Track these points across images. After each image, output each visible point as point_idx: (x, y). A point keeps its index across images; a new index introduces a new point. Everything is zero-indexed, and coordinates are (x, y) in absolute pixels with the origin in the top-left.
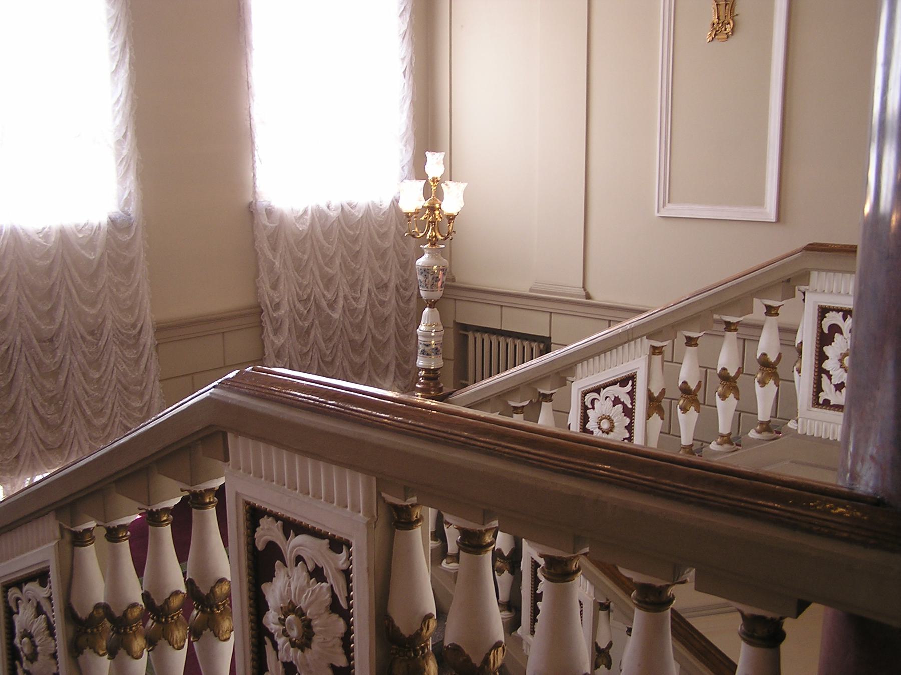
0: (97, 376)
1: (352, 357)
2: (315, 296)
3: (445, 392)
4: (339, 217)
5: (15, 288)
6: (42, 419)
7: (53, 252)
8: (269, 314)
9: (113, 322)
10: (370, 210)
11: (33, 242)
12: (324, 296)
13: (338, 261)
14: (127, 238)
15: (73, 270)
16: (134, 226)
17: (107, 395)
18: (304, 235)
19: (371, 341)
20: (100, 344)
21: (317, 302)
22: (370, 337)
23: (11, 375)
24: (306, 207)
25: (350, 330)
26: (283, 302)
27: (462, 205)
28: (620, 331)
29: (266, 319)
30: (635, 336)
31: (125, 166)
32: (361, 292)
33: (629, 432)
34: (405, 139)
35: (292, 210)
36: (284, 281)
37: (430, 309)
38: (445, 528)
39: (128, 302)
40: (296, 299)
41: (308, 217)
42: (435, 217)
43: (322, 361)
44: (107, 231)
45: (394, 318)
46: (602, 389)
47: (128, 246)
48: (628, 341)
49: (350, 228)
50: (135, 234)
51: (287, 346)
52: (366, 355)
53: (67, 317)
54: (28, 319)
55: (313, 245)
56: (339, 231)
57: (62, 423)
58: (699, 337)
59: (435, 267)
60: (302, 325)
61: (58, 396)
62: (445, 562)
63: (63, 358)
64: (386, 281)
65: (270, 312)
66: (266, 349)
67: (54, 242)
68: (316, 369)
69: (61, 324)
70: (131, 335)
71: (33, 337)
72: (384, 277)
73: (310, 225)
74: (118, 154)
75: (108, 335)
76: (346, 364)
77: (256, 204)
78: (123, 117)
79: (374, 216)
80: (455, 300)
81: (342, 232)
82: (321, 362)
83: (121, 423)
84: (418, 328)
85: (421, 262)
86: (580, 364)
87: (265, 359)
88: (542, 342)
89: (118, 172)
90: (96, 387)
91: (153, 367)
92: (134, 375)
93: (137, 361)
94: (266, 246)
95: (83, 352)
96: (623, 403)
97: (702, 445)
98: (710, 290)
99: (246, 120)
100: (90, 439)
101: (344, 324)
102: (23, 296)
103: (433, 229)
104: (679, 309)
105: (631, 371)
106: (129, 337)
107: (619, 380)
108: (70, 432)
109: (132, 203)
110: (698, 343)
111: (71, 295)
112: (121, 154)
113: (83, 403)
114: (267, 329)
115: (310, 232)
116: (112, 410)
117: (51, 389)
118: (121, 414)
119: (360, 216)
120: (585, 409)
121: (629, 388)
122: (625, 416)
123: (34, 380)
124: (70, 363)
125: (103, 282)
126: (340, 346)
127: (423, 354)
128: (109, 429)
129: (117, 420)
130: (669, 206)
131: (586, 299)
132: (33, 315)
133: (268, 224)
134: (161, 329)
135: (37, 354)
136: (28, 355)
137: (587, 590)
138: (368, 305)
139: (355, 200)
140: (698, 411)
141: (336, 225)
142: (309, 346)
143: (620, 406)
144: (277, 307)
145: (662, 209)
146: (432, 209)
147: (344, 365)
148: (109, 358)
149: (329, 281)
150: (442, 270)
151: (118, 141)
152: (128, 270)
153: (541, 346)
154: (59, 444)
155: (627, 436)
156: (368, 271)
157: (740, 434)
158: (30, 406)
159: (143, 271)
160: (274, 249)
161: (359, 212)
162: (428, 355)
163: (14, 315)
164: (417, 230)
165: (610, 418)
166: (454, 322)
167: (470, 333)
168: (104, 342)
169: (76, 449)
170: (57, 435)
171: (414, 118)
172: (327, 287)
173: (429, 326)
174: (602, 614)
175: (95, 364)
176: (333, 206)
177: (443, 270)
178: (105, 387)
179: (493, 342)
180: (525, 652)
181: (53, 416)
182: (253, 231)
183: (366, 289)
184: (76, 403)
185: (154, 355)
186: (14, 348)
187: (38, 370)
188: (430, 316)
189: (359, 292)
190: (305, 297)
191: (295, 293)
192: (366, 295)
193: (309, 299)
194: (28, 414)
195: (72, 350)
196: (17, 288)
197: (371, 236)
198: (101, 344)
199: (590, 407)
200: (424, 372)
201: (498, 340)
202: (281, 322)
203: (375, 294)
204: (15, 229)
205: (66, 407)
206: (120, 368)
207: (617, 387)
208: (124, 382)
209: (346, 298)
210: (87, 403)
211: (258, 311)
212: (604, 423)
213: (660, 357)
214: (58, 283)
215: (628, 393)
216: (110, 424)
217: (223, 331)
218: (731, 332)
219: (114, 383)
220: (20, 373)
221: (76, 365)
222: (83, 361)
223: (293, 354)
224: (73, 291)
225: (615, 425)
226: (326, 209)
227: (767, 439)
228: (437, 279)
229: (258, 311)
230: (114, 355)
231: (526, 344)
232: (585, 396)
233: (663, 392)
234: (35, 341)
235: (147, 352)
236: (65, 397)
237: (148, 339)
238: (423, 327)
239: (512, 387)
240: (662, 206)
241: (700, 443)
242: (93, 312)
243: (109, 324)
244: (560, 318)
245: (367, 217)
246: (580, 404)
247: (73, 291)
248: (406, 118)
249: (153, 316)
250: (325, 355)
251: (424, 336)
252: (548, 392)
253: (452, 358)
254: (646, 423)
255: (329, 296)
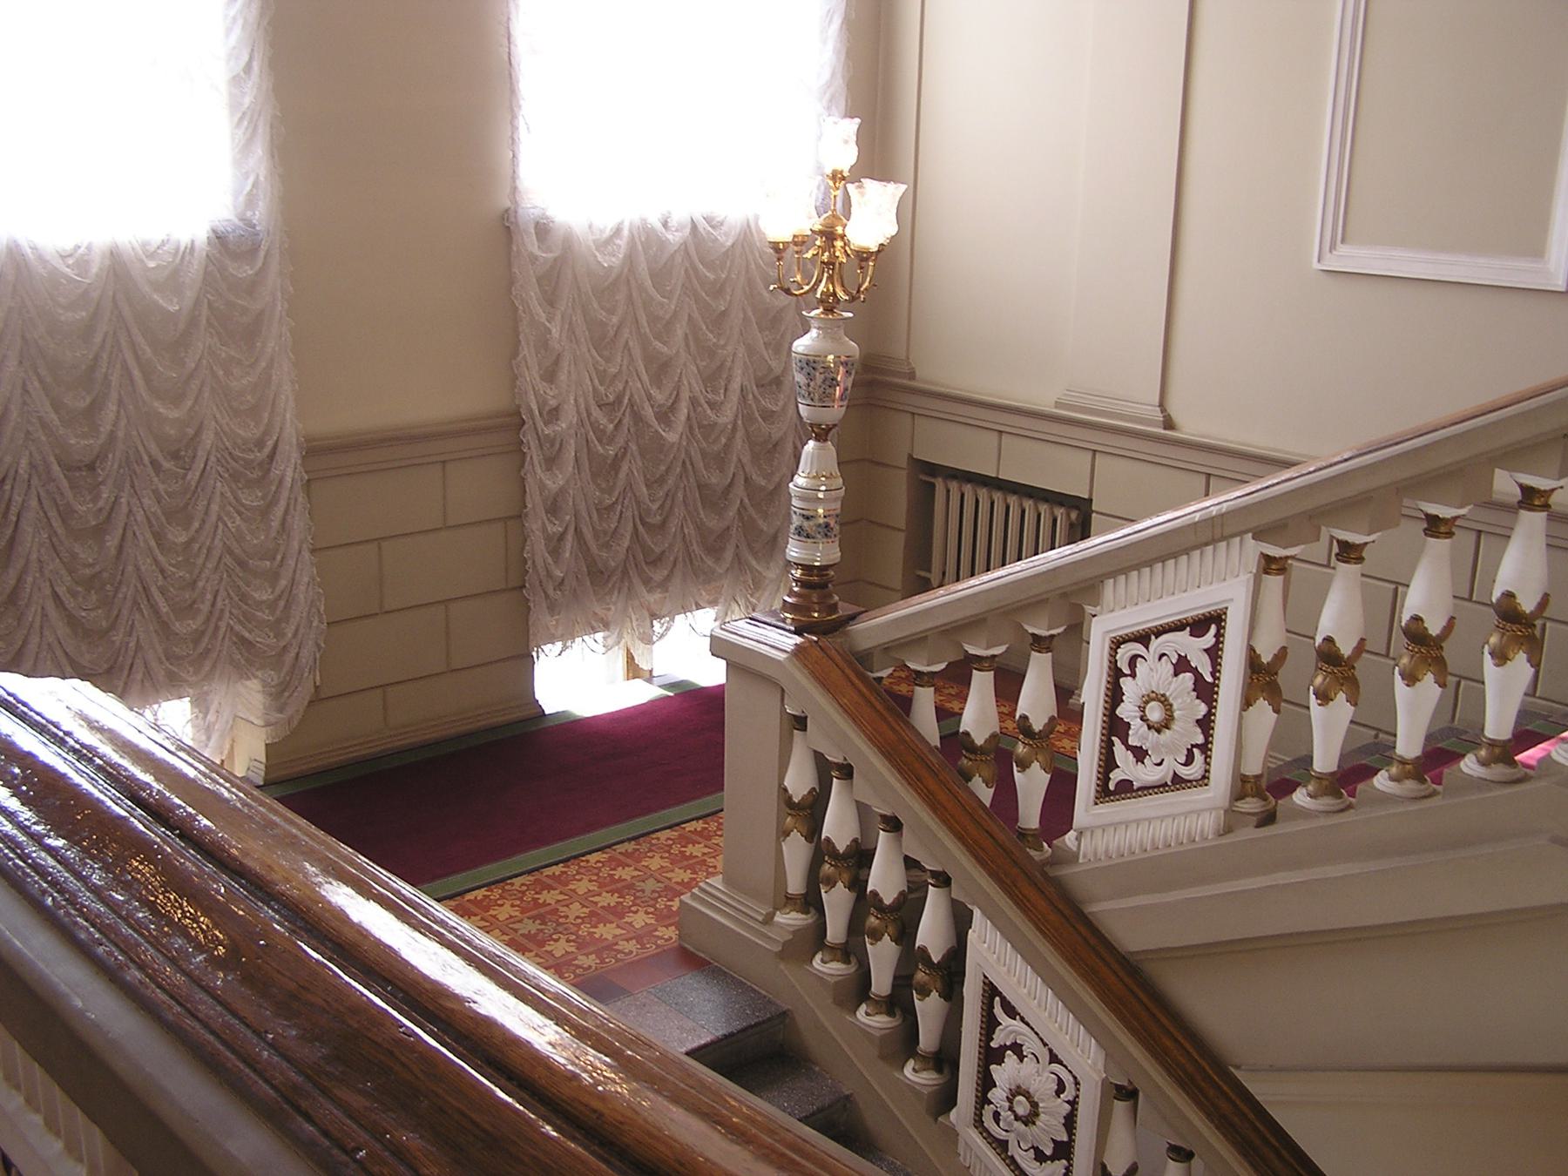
0: (182, 539)
1: (702, 516)
2: (632, 395)
3: (841, 613)
4: (685, 243)
5: (16, 363)
6: (72, 621)
7: (95, 295)
8: (536, 428)
9: (217, 434)
10: (750, 231)
11: (54, 272)
12: (650, 397)
13: (680, 330)
14: (246, 272)
15: (135, 331)
16: (264, 247)
17: (203, 575)
18: (614, 276)
19: (742, 487)
20: (189, 477)
21: (635, 408)
22: (740, 481)
23: (9, 532)
24: (619, 220)
25: (700, 465)
26: (566, 406)
27: (892, 229)
28: (1197, 517)
29: (529, 437)
30: (1227, 532)
31: (247, 129)
32: (726, 390)
33: (1203, 733)
34: (828, 96)
35: (590, 227)
36: (569, 365)
37: (818, 443)
38: (823, 891)
39: (249, 397)
40: (592, 402)
41: (622, 242)
42: (834, 252)
43: (641, 520)
44: (207, 256)
45: (791, 444)
46: (1153, 637)
47: (252, 287)
48: (1214, 541)
49: (709, 265)
50: (264, 264)
51: (571, 492)
52: (732, 513)
53: (123, 422)
54: (44, 425)
55: (630, 297)
56: (686, 271)
57: (113, 627)
58: (1366, 544)
59: (831, 358)
60: (602, 451)
61: (105, 575)
62: (818, 957)
63: (114, 503)
64: (778, 371)
65: (538, 425)
66: (528, 496)
67: (97, 275)
68: (628, 538)
69: (112, 436)
70: (252, 461)
71: (52, 459)
72: (773, 364)
73: (625, 257)
74: (234, 105)
75: (207, 459)
76: (690, 530)
77: (516, 212)
78: (243, 28)
79: (758, 244)
80: (913, 414)
81: (691, 272)
82: (640, 528)
83: (232, 628)
84: (792, 481)
85: (802, 345)
86: (1112, 581)
87: (526, 515)
88: (1077, 508)
89: (233, 139)
90: (180, 559)
91: (299, 523)
92: (257, 538)
93: (265, 512)
94: (533, 295)
95: (156, 492)
96: (1195, 671)
97: (1376, 736)
98: (1397, 444)
99: (501, 46)
100: (167, 659)
101: (688, 453)
102: (35, 378)
103: (830, 279)
104: (1326, 480)
105: (1216, 604)
106: (248, 464)
107: (1191, 621)
108: (128, 643)
109: (260, 203)
110: (1364, 555)
111: (132, 380)
112: (241, 104)
113: (154, 589)
114: (531, 457)
115: (626, 270)
116: (213, 605)
117: (91, 560)
118: (231, 613)
119: (729, 243)
120: (1116, 674)
121: (1209, 639)
122: (1198, 698)
123: (57, 543)
124: (130, 511)
125: (198, 357)
126: (680, 495)
127: (799, 534)
128: (206, 640)
129: (223, 625)
130: (1342, 249)
131: (1165, 428)
132: (53, 417)
133: (538, 253)
134: (314, 450)
135: (62, 494)
136: (43, 494)
137: (1092, 1054)
138: (740, 416)
139: (720, 213)
140: (1353, 701)
141: (679, 259)
142: (616, 493)
143: (1189, 675)
144: (553, 414)
145: (1329, 255)
146: (829, 235)
147: (686, 531)
148: (209, 504)
149: (660, 369)
150: (842, 363)
151: (234, 78)
152: (251, 333)
153: (1074, 515)
154: (106, 666)
155: (1200, 739)
156: (741, 352)
157: (1456, 722)
158: (48, 591)
159: (281, 336)
160: (550, 301)
161: (726, 234)
162: (808, 536)
163: (14, 414)
164: (798, 278)
165: (1166, 700)
166: (910, 456)
167: (940, 480)
168: (198, 474)
169: (139, 676)
170: (101, 649)
171: (847, 53)
172: (657, 380)
173: (814, 477)
174: (1120, 1107)
175: (179, 514)
176: (673, 223)
177: (845, 364)
178: (200, 561)
179: (981, 500)
180: (961, 1158)
181: (93, 614)
182: (509, 265)
183: (735, 386)
184: (140, 589)
185: (300, 499)
186: (15, 479)
187: (63, 521)
188: (817, 457)
189: (722, 391)
190: (612, 398)
191: (591, 389)
192: (734, 397)
193: (619, 399)
194: (43, 608)
195: (133, 487)
196: (21, 362)
197: (750, 282)
198: (193, 476)
199: (1127, 671)
200: (799, 571)
201: (991, 497)
202: (561, 445)
203: (754, 396)
204: (18, 246)
205: (120, 595)
206: (230, 525)
207: (1183, 637)
208: (238, 551)
209: (694, 402)
210: (163, 591)
211: (513, 421)
212: (1152, 708)
213: (1280, 578)
214: (105, 356)
215: (1206, 650)
216: (210, 630)
217: (442, 458)
218: (1438, 537)
219: (216, 553)
220: (27, 527)
221: (140, 516)
222: (155, 508)
223: (582, 507)
224: (136, 373)
225: (1176, 714)
226: (658, 226)
227: (1504, 779)
228: (833, 383)
229: (513, 421)
230: (217, 498)
231: (1043, 508)
232: (1119, 647)
233: (1282, 655)
234: (56, 468)
235: (285, 494)
236: (119, 577)
237: (289, 468)
238: (800, 480)
239: (972, 616)
240: (1328, 249)
241: (1373, 733)
242: (174, 414)
243: (208, 439)
244: (1109, 460)
245: (743, 246)
246: (1106, 664)
247: (136, 373)
248: (831, 53)
249: (301, 426)
250: (648, 510)
251: (801, 498)
252: (1044, 633)
253: (902, 524)
254: (1241, 717)
255: (660, 397)
